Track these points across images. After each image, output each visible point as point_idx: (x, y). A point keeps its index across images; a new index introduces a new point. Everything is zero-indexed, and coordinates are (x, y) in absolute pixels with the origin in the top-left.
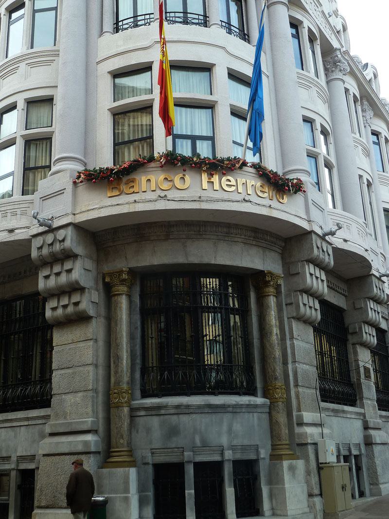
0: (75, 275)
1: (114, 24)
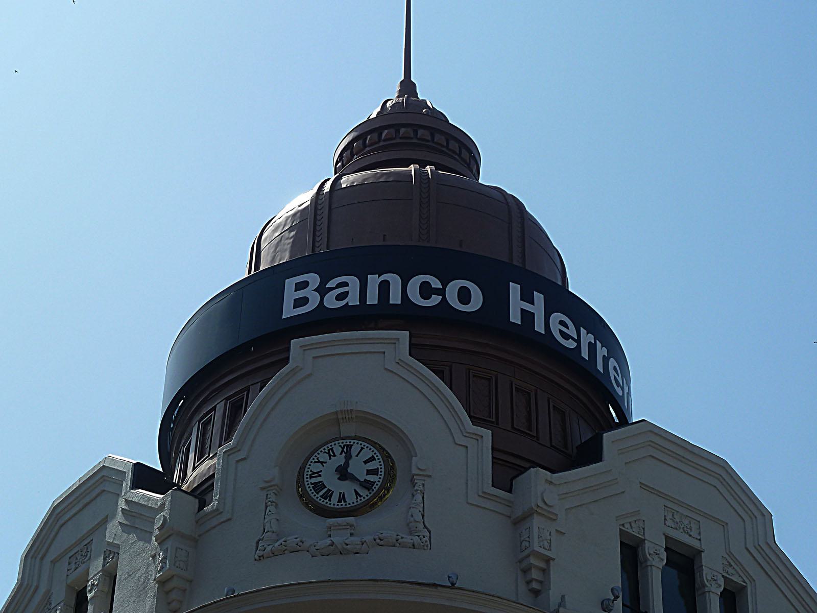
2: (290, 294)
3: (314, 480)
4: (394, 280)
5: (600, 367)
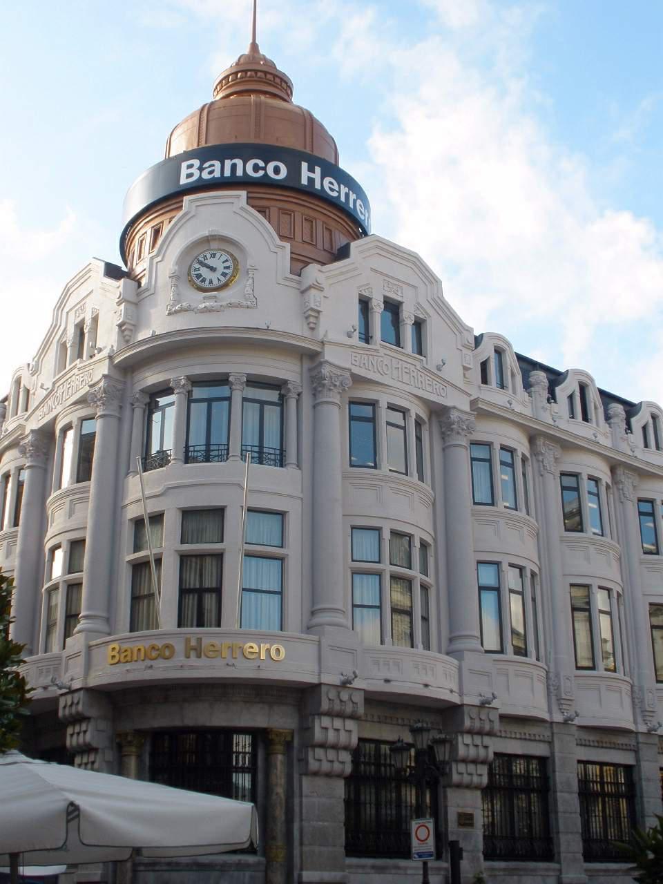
0: (88, 737)
1: (320, 392)
2: (184, 171)
3: (196, 273)
4: (239, 162)
5: (351, 206)
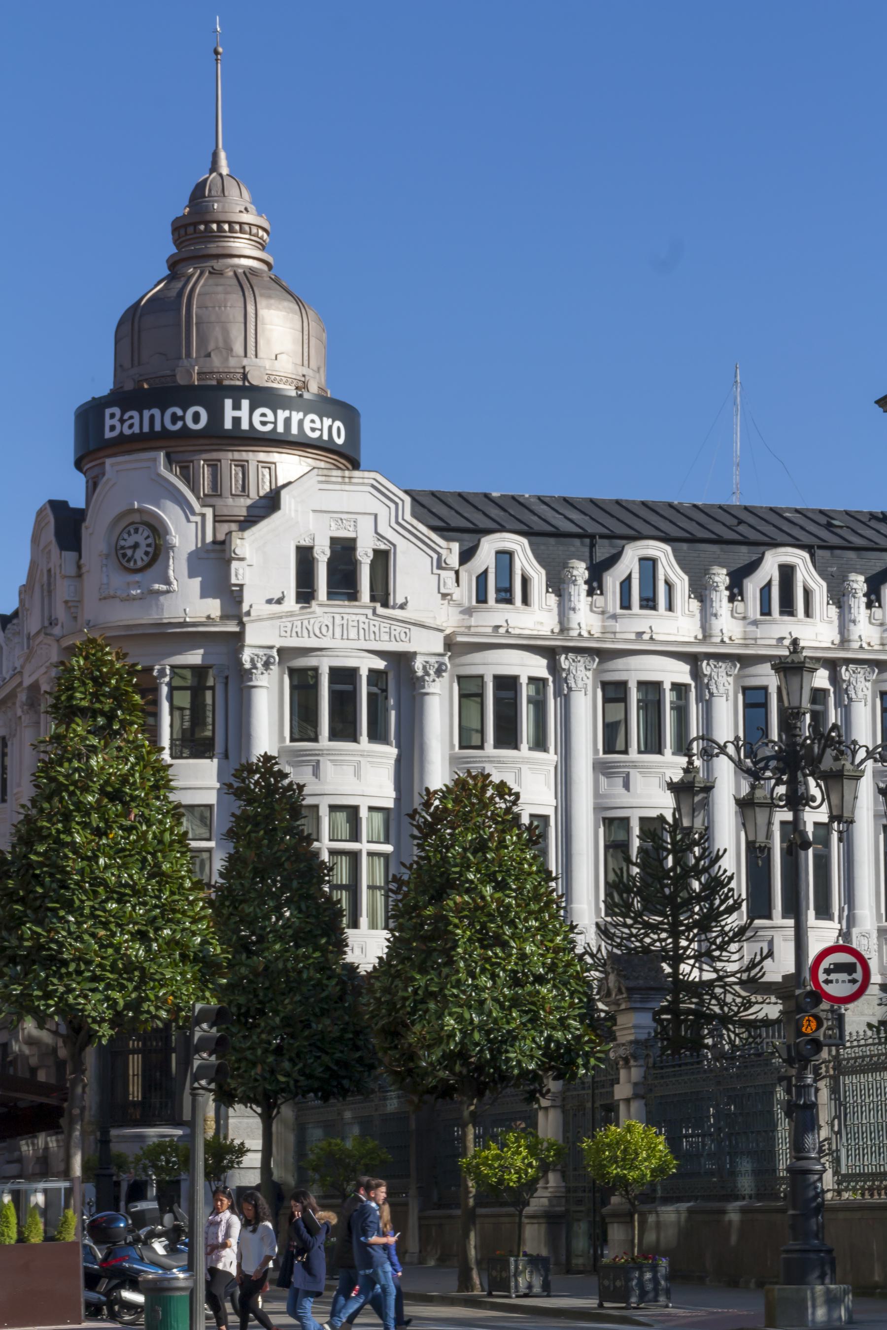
4: (156, 412)
